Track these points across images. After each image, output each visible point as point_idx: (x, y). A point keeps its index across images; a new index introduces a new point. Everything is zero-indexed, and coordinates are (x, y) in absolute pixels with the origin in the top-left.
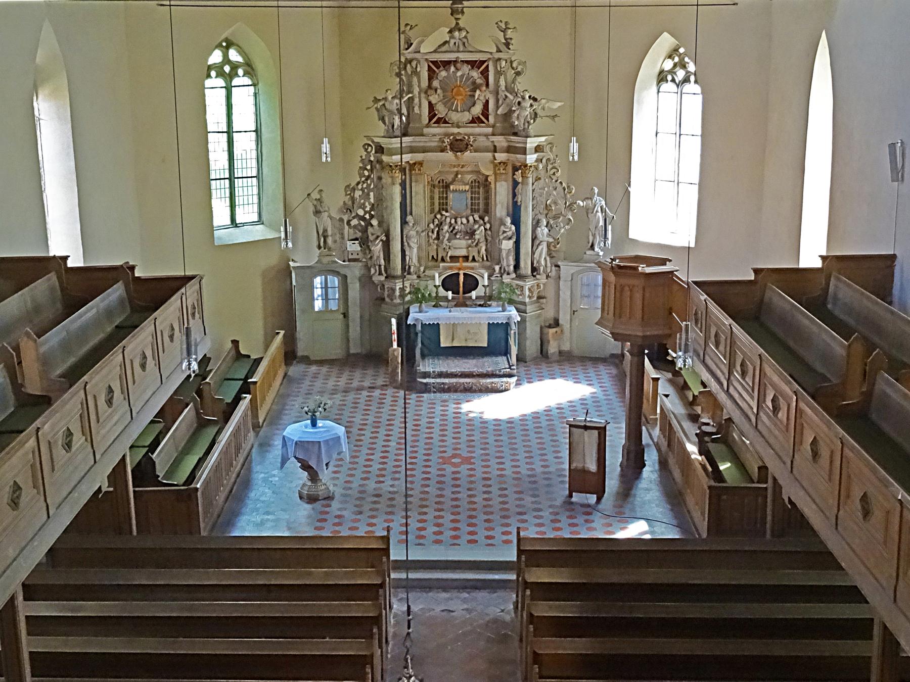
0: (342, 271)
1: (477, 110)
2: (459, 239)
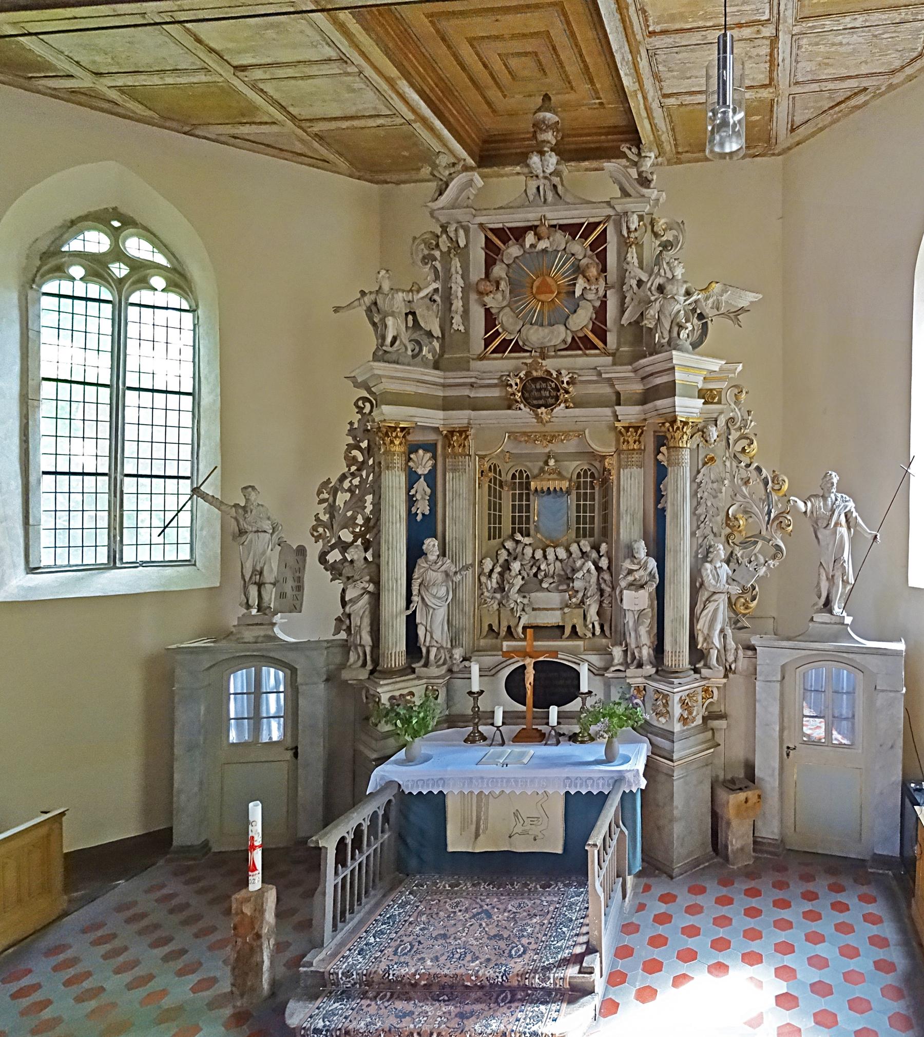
0: (289, 657)
1: (582, 319)
2: (547, 590)
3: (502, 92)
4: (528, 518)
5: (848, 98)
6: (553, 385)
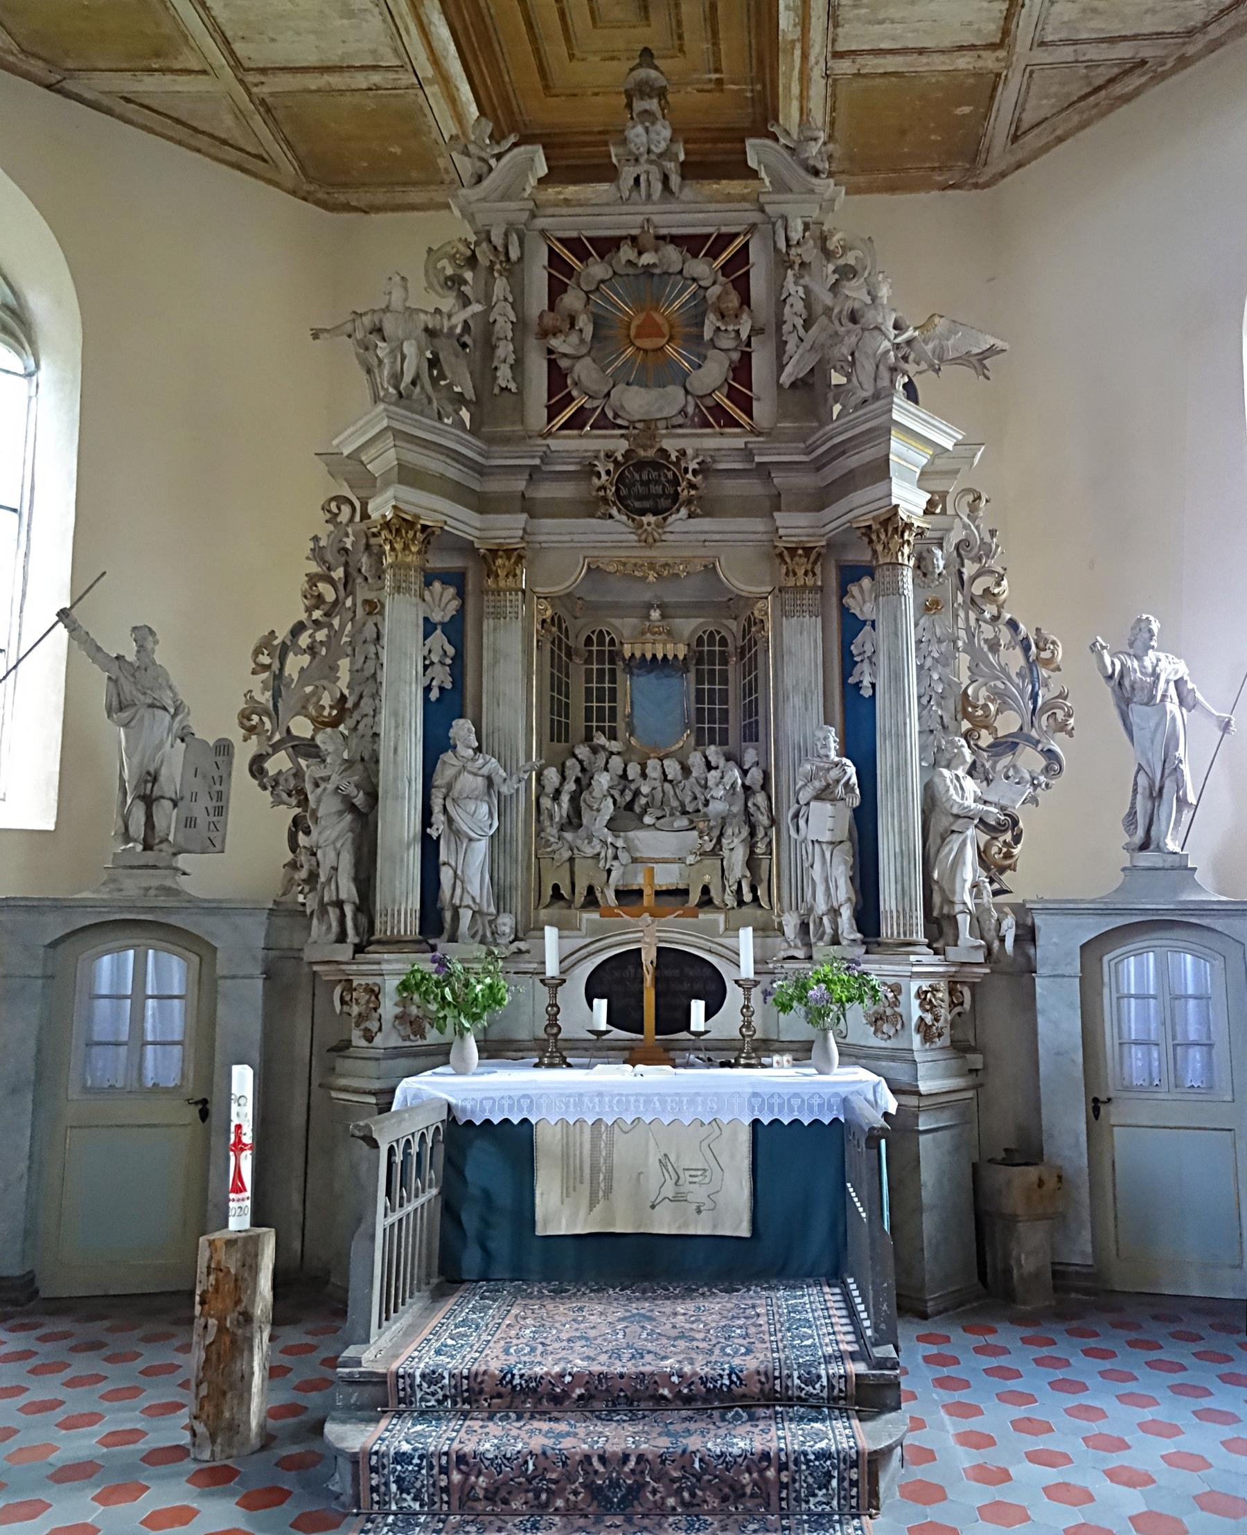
1: (711, 375)
3: (570, 48)
4: (613, 710)
5: (1112, 81)
6: (670, 475)
